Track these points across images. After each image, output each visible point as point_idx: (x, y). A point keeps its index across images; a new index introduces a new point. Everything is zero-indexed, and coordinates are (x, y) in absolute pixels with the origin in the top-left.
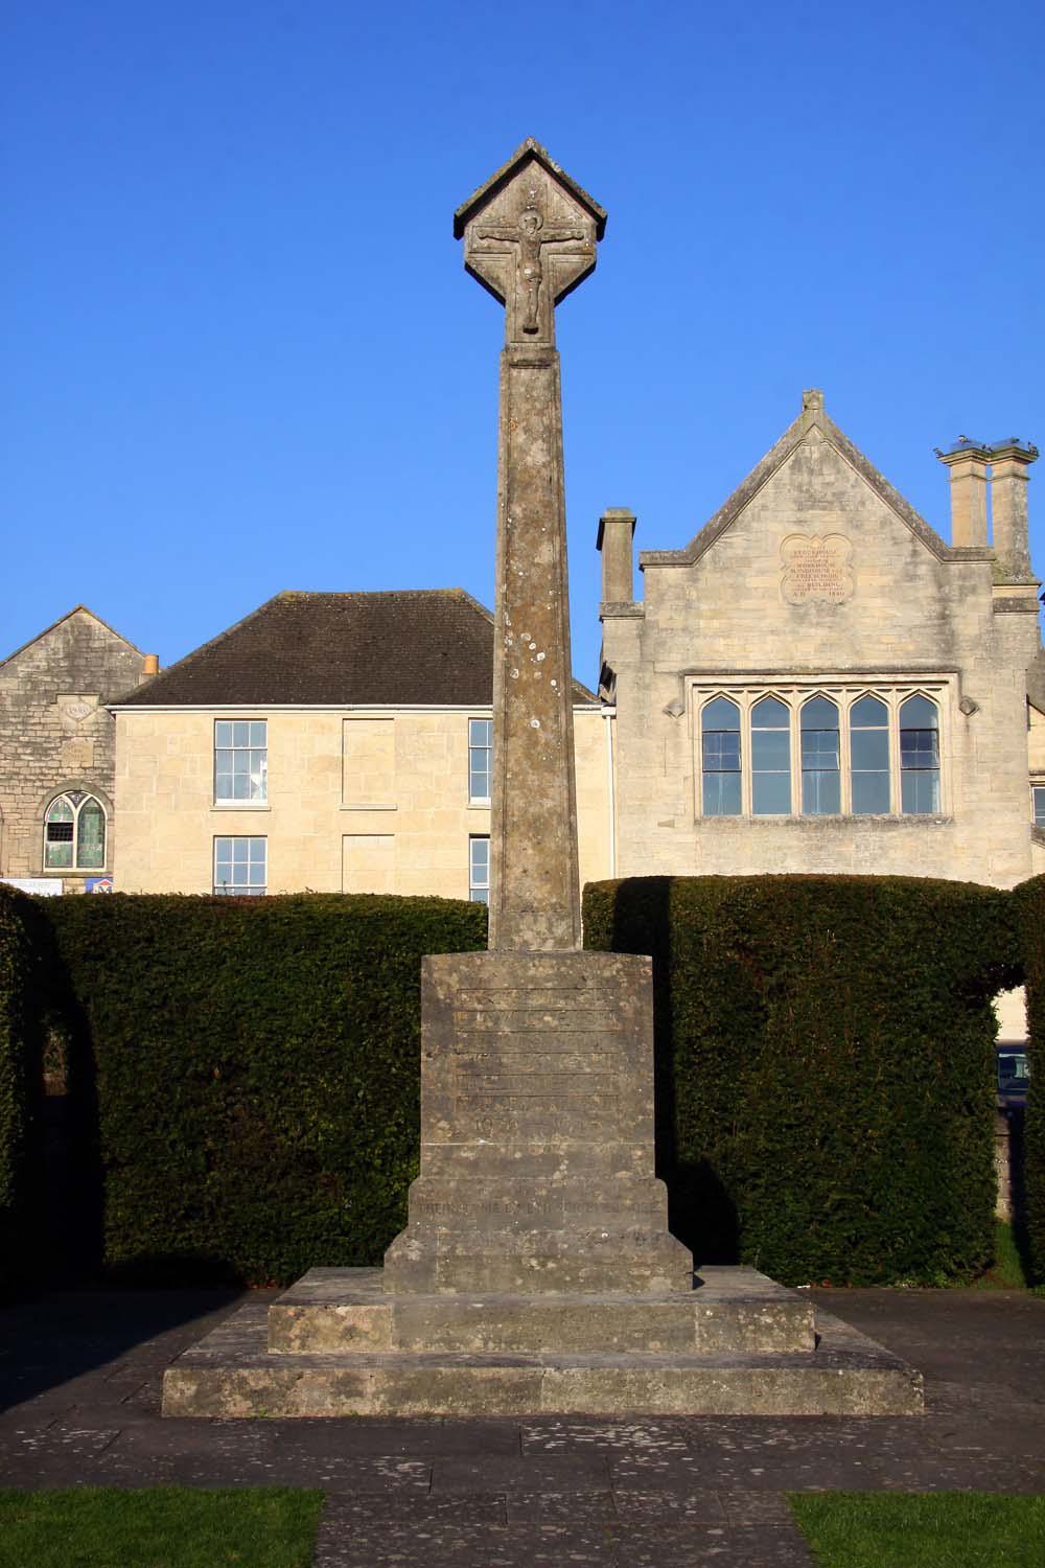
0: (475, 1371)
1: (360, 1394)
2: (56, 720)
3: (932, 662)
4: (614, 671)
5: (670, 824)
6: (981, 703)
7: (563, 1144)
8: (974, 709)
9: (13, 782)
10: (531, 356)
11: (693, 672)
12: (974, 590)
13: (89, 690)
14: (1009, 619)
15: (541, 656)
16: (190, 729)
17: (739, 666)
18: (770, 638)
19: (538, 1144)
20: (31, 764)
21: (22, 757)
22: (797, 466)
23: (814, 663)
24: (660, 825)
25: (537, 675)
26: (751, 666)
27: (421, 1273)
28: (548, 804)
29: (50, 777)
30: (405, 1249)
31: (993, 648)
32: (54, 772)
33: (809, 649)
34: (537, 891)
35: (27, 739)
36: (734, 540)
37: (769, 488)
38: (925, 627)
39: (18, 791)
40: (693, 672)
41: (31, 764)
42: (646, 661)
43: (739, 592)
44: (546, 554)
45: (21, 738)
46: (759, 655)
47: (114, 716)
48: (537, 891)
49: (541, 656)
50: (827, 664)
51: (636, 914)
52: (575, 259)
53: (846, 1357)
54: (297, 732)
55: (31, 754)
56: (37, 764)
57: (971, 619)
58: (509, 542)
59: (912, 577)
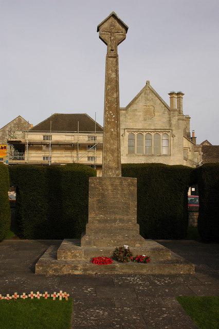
1: (77, 270)
3: (168, 128)
7: (118, 217)
8: (175, 136)
10: (112, 55)
11: (126, 129)
12: (175, 116)
13: (21, 130)
14: (181, 122)
15: (114, 116)
17: (135, 128)
19: (113, 217)
22: (145, 93)
23: (147, 128)
25: (113, 120)
27: (89, 243)
28: (115, 147)
30: (85, 239)
31: (178, 127)
34: (114, 165)
37: (140, 97)
40: (126, 129)
43: (135, 115)
44: (115, 96)
46: (139, 126)
48: (114, 165)
49: (114, 116)
51: (128, 170)
52: (122, 36)
53: (178, 262)
57: (174, 121)
58: (62, 145)
59: (164, 113)
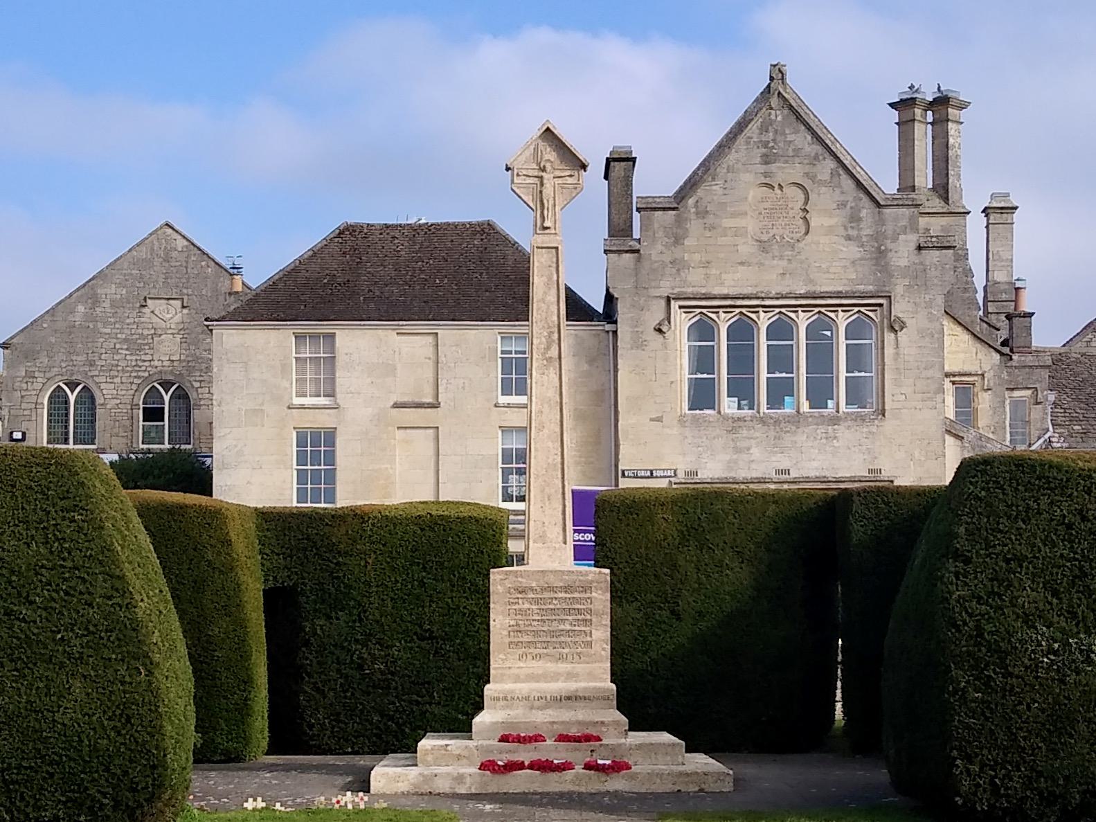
0: (534, 796)
2: (148, 320)
4: (616, 296)
5: (659, 419)
6: (909, 322)
9: (113, 373)
16: (274, 343)
18: (740, 268)
20: (128, 357)
21: (120, 351)
24: (652, 420)
26: (725, 291)
29: (143, 368)
32: (147, 364)
33: (770, 278)
35: (124, 336)
36: (714, 187)
38: (865, 259)
39: (117, 380)
41: (128, 357)
42: (639, 288)
45: (119, 336)
46: (732, 282)
47: (211, 330)
50: (785, 291)
54: (357, 343)
55: (127, 349)
56: (134, 358)
